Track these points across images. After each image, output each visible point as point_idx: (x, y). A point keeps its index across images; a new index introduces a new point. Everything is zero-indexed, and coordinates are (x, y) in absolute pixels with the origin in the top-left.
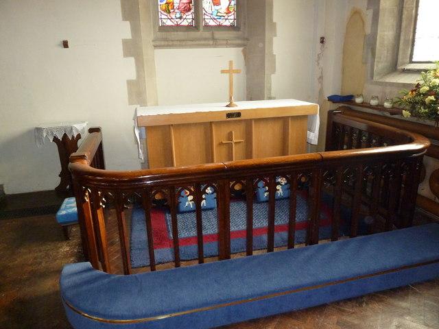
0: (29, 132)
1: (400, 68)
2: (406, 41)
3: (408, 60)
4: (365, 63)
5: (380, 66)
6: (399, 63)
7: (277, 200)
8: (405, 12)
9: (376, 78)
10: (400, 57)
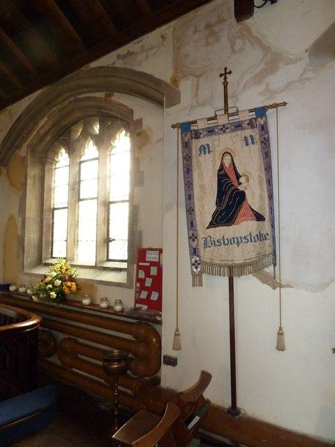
0: (284, 345)
1: (44, 262)
2: (47, 242)
3: (50, 256)
4: (18, 257)
5: (29, 260)
6: (43, 258)
7: (127, 201)
8: (45, 222)
9: (26, 270)
10: (43, 253)
